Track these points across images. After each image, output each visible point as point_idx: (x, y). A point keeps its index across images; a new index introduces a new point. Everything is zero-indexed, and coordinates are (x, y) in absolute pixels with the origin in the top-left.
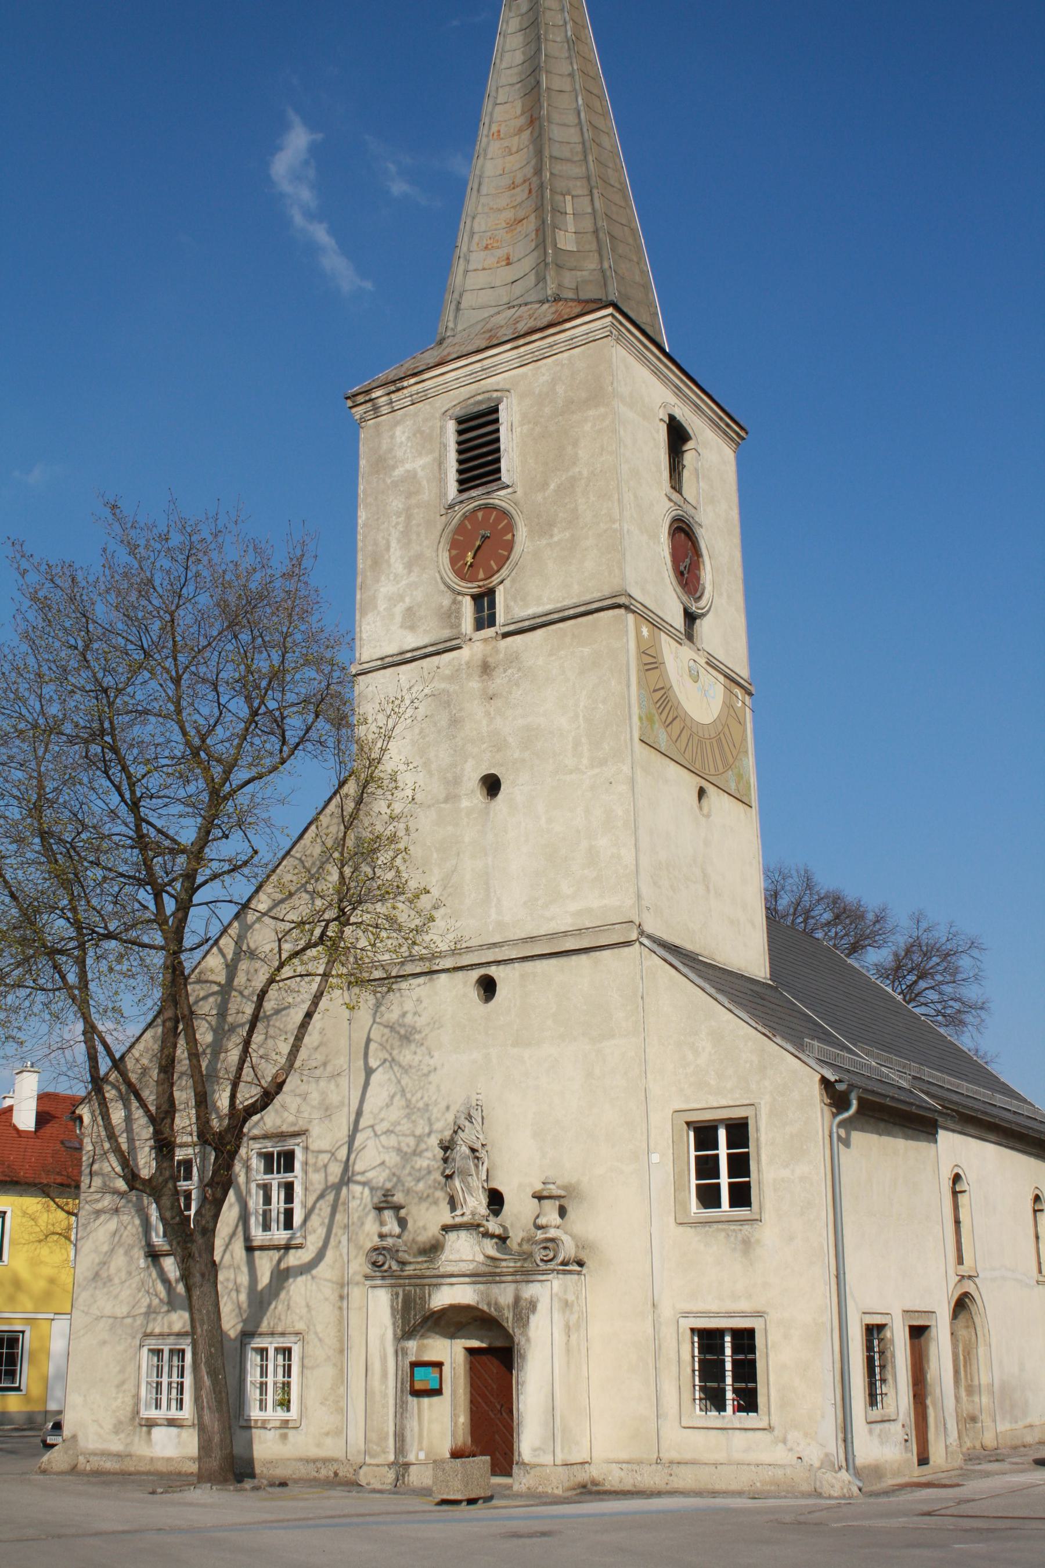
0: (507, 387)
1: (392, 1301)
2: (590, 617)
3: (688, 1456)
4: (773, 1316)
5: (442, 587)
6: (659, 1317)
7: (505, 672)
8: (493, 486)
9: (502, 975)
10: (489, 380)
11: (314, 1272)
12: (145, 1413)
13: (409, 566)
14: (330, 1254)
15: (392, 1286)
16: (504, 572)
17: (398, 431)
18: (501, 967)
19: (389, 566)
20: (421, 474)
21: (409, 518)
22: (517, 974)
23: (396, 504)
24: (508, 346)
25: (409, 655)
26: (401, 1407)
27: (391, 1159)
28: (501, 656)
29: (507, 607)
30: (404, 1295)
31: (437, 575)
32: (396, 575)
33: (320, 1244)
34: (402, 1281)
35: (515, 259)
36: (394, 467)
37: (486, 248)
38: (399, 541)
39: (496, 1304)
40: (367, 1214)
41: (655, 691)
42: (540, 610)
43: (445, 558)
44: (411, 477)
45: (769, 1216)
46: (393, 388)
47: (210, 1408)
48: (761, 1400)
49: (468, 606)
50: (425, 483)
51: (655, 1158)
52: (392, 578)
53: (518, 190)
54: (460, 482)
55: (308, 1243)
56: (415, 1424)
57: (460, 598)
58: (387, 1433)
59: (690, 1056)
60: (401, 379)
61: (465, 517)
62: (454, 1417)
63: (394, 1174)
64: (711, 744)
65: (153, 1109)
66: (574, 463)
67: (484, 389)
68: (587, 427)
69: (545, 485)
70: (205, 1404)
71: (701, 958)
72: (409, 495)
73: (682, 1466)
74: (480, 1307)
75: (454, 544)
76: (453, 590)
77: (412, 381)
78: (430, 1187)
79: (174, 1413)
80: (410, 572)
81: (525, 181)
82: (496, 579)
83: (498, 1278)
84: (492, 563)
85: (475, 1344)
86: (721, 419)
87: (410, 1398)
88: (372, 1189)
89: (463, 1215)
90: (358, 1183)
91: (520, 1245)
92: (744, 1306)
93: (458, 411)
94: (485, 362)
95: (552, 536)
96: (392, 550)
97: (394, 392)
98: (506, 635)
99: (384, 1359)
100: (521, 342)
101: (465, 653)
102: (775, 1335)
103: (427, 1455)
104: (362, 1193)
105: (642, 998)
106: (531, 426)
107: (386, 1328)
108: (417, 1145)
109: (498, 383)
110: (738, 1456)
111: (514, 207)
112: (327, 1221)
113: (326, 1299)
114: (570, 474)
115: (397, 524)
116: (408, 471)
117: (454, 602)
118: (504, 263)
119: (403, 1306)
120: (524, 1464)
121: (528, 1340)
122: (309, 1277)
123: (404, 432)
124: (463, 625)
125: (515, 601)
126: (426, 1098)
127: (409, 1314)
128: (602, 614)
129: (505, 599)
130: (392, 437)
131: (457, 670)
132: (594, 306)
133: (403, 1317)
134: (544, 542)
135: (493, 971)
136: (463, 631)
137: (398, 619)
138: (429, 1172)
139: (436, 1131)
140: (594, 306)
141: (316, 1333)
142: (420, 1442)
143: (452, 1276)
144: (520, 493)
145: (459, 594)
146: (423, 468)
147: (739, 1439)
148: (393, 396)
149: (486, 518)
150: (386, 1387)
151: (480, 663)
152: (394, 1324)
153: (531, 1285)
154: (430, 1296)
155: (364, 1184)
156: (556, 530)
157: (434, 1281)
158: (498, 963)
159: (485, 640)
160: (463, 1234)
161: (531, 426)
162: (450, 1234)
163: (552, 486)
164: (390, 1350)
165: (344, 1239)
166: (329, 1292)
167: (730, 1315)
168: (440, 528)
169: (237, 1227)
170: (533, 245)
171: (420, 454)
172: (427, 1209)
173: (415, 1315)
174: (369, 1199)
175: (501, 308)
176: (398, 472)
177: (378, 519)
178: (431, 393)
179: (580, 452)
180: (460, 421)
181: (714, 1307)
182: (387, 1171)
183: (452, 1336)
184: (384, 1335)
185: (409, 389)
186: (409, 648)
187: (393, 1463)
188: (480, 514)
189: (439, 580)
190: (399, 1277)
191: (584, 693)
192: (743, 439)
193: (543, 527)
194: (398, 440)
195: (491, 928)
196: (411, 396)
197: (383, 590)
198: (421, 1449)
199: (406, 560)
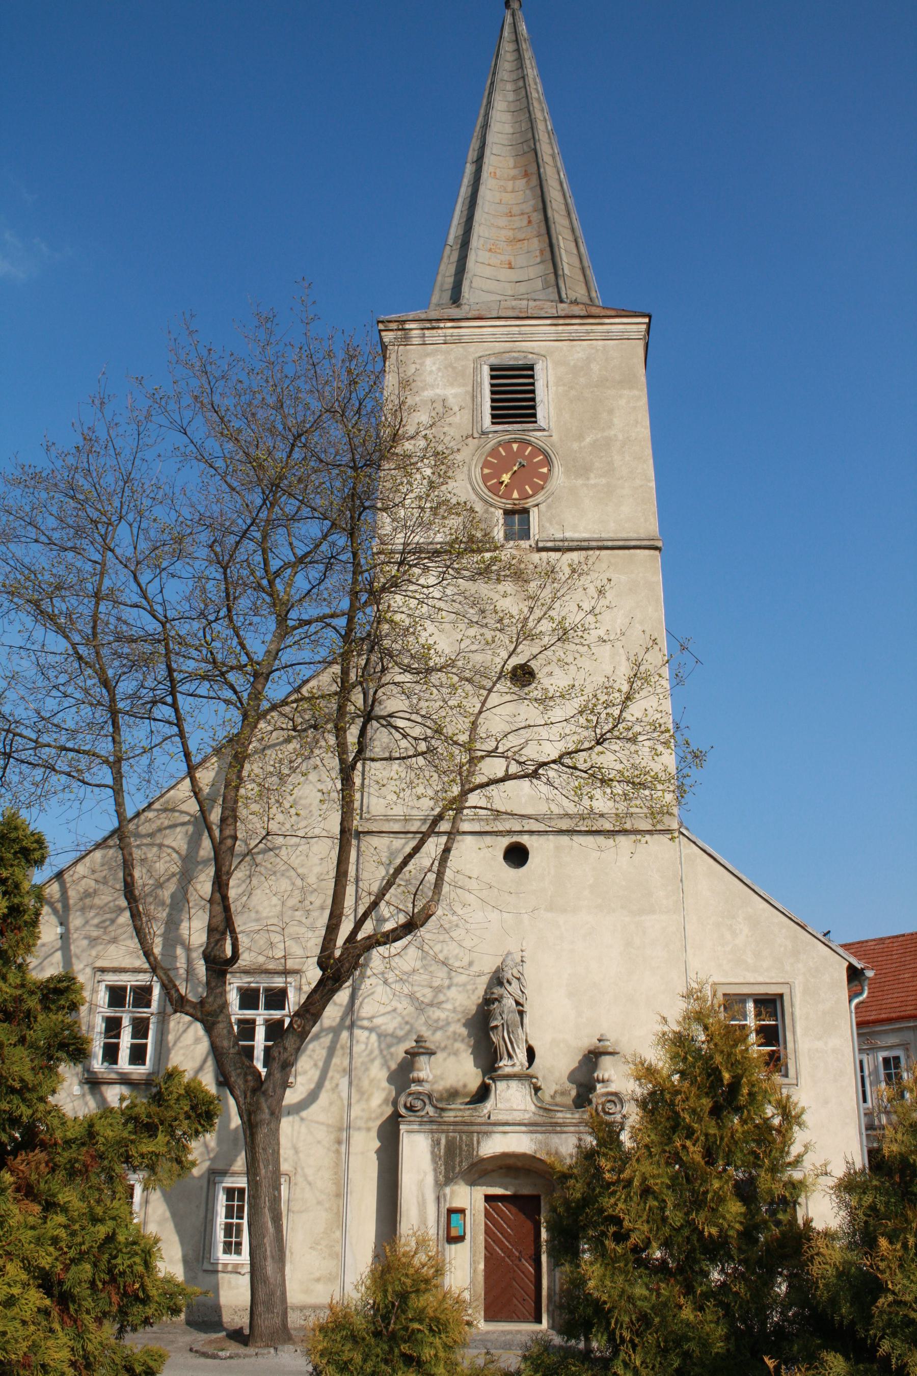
0: (543, 353)
1: (433, 1147)
2: (626, 552)
9: (535, 845)
10: (523, 343)
11: (304, 1114)
14: (324, 1097)
15: (432, 1132)
16: (539, 498)
18: (535, 838)
22: (552, 846)
24: (548, 322)
27: (404, 1006)
30: (448, 1142)
31: (469, 486)
33: (312, 1086)
34: (445, 1127)
36: (424, 389)
39: (557, 1153)
40: (373, 1060)
46: (428, 325)
47: (273, 1257)
54: (494, 416)
55: (298, 1082)
60: (438, 320)
61: (499, 444)
62: (473, 1263)
63: (407, 1023)
65: (360, 936)
67: (519, 349)
68: (622, 402)
69: (580, 437)
70: (268, 1253)
74: (538, 1156)
77: (449, 324)
78: (448, 1038)
82: (530, 502)
83: (558, 1129)
85: (498, 1191)
87: (447, 1246)
88: (379, 1036)
89: (513, 1065)
90: (362, 1028)
91: (553, 1097)
93: (494, 361)
94: (523, 328)
95: (588, 479)
97: (428, 329)
99: (422, 1205)
100: (561, 321)
104: (368, 1038)
105: (681, 881)
106: (566, 388)
107: (425, 1173)
108: (435, 996)
109: (533, 348)
111: (513, 229)
112: (321, 1064)
113: (319, 1142)
114: (606, 434)
117: (486, 511)
119: (446, 1152)
122: (297, 1118)
125: (551, 524)
126: (445, 952)
127: (453, 1160)
128: (638, 551)
132: (613, 313)
133: (446, 1164)
134: (580, 482)
135: (525, 840)
138: (448, 1024)
139: (457, 985)
140: (613, 313)
141: (305, 1177)
143: (506, 1124)
144: (555, 438)
145: (491, 505)
146: (455, 396)
148: (426, 332)
149: (521, 451)
152: (435, 1170)
154: (478, 1143)
155: (371, 1030)
156: (592, 475)
157: (490, 1128)
158: (531, 832)
160: (514, 1084)
161: (566, 388)
162: (498, 1083)
163: (588, 440)
165: (344, 1082)
166: (324, 1136)
169: (205, 1061)
170: (538, 260)
171: (452, 385)
172: (445, 1059)
173: (461, 1162)
174: (376, 1044)
178: (465, 339)
179: (615, 420)
182: (399, 1019)
184: (423, 1180)
185: (444, 331)
188: (515, 446)
190: (440, 1123)
193: (582, 470)
195: (523, 800)
196: (445, 336)
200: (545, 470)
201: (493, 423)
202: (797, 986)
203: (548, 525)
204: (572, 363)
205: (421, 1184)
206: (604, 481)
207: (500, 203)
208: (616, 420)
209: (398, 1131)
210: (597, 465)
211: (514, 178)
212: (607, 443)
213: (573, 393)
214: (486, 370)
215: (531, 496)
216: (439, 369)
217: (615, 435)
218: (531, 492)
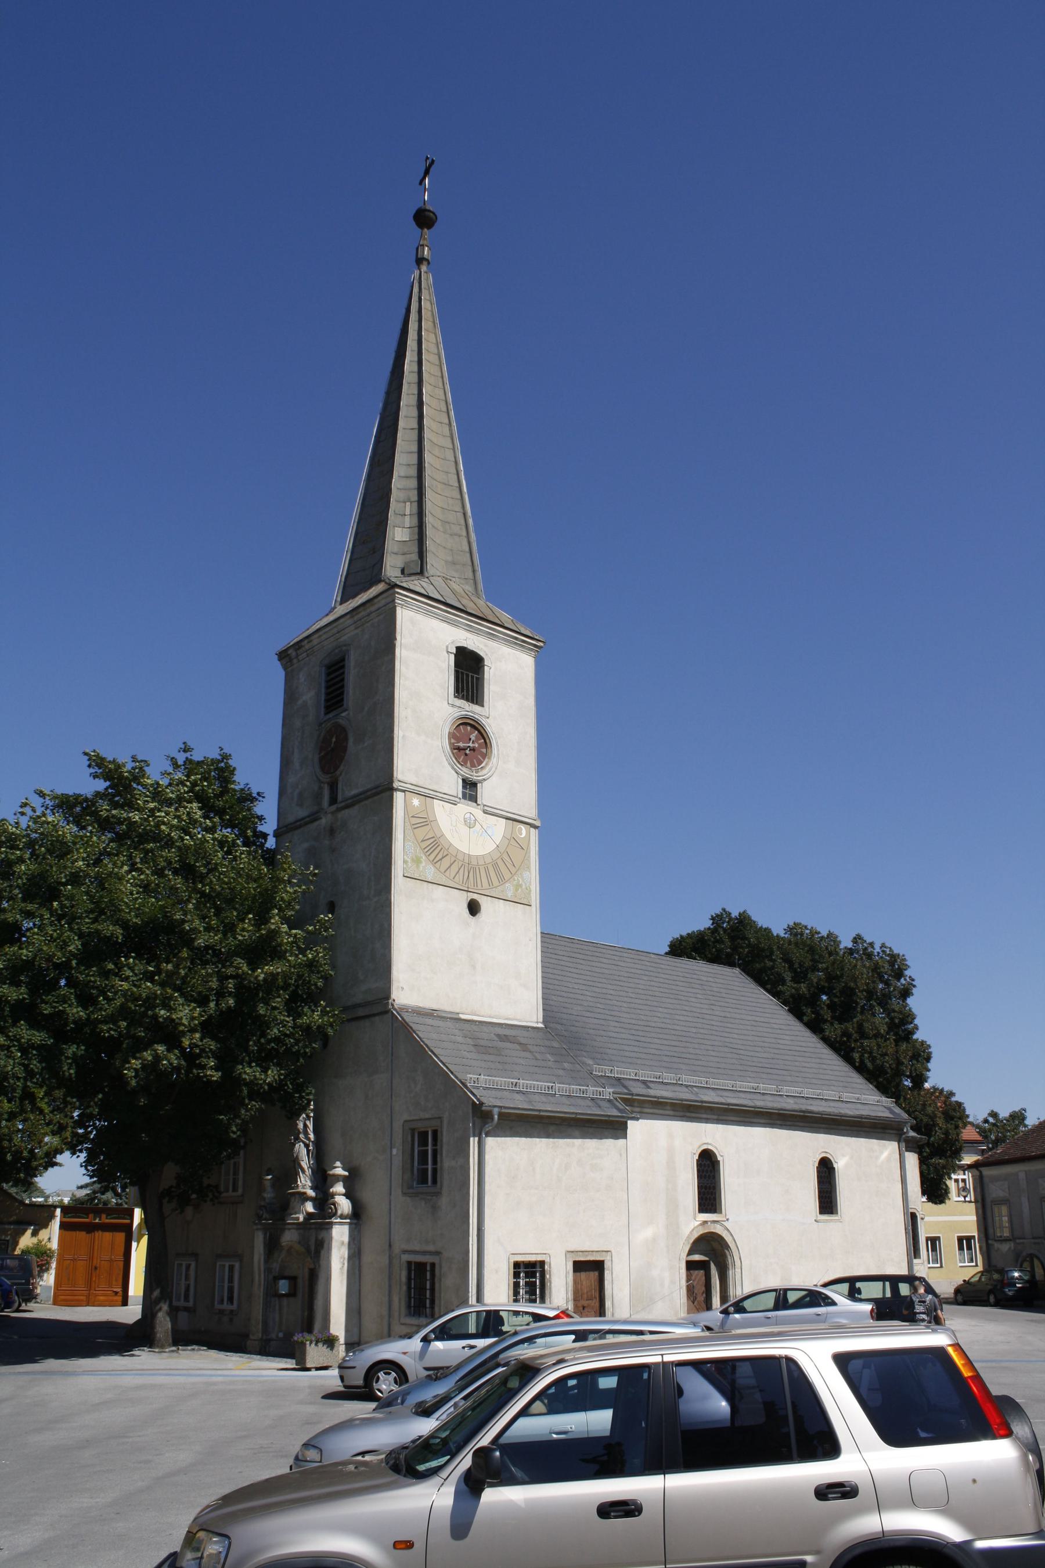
8: (340, 709)
12: (217, 1306)
41: (422, 841)
45: (445, 1191)
51: (394, 1151)
57: (322, 785)
64: (487, 870)
71: (462, 1016)
76: (319, 780)
79: (186, 1304)
86: (516, 638)
92: (431, 1248)
121: (319, 1266)
145: (322, 782)
163: (366, 709)
176: (300, 702)
192: (541, 647)
198: (281, 1331)
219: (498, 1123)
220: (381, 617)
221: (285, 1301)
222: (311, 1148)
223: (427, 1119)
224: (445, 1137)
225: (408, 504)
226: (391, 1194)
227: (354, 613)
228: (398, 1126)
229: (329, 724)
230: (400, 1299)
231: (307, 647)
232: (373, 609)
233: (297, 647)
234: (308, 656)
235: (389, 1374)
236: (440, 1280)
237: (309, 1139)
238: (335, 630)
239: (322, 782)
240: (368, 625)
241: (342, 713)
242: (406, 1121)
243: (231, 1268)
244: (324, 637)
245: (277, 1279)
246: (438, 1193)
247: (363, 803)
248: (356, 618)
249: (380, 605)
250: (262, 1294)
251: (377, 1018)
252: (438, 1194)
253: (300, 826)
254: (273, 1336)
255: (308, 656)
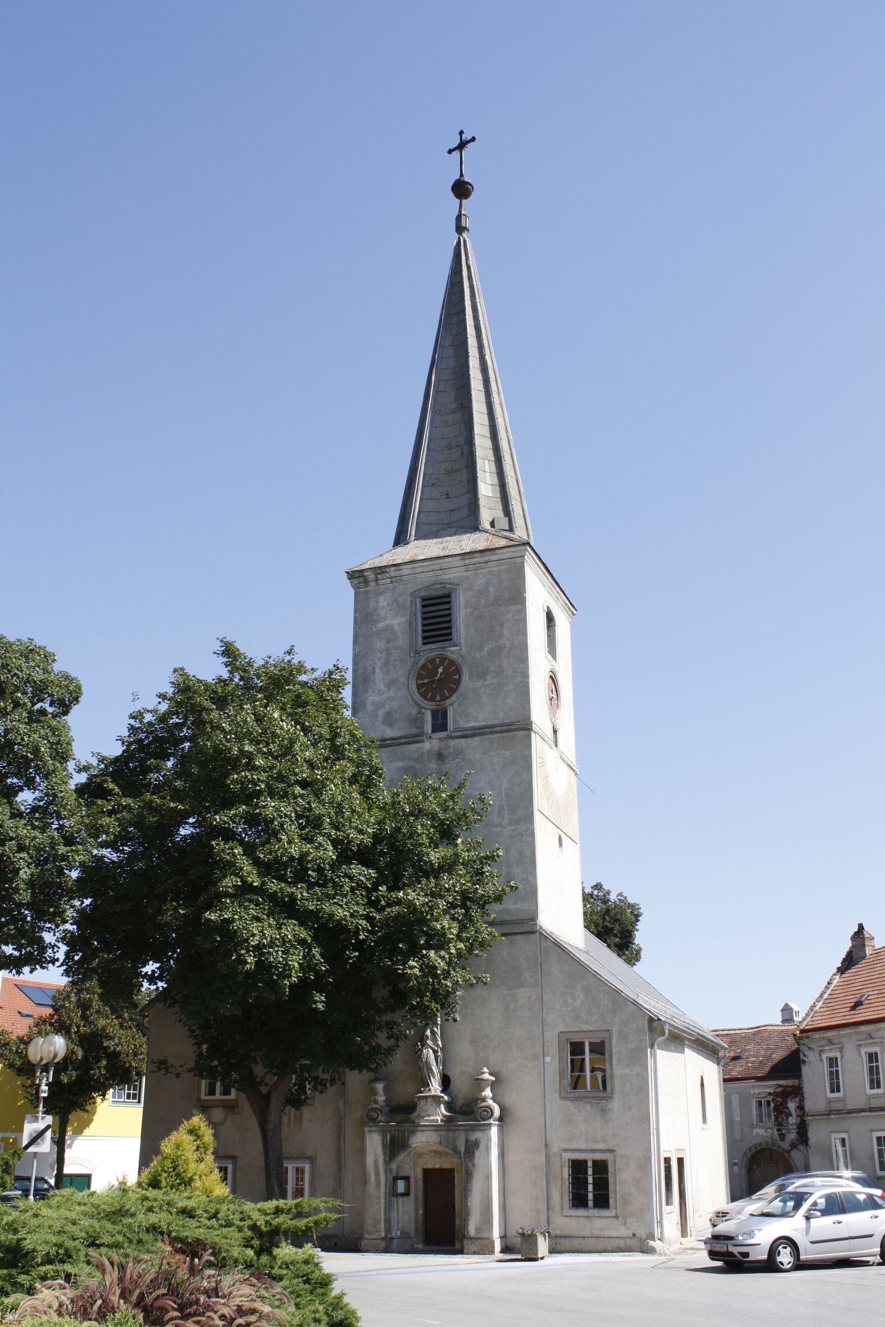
1: (383, 1140)
3: (567, 1233)
4: (619, 1152)
5: (411, 702)
6: (549, 1152)
7: (453, 760)
13: (389, 686)
16: (454, 698)
17: (381, 598)
19: (375, 683)
20: (396, 628)
21: (389, 655)
23: (380, 645)
25: (389, 742)
26: (389, 1204)
28: (451, 750)
29: (455, 721)
31: (408, 694)
32: (379, 691)
35: (452, 496)
36: (378, 622)
37: (433, 485)
38: (381, 669)
42: (477, 724)
43: (413, 685)
44: (390, 629)
45: (616, 1095)
48: (611, 1201)
49: (428, 717)
50: (399, 634)
51: (548, 1059)
52: (376, 691)
53: (453, 450)
54: (424, 638)
56: (395, 1214)
58: (380, 1219)
59: (570, 1001)
62: (416, 1210)
66: (501, 637)
68: (510, 616)
69: (481, 649)
72: (388, 641)
73: (563, 1239)
75: (419, 677)
76: (419, 705)
80: (389, 689)
81: (458, 446)
82: (448, 702)
84: (446, 691)
93: (423, 593)
95: (485, 680)
96: (377, 674)
98: (452, 738)
101: (427, 745)
102: (620, 1163)
103: (401, 1233)
109: (450, 579)
110: (597, 1233)
111: (451, 461)
114: (498, 643)
115: (380, 658)
116: (388, 626)
117: (420, 712)
118: (445, 497)
120: (471, 1238)
121: (474, 1165)
123: (385, 600)
124: (425, 728)
125: (461, 718)
129: (454, 715)
130: (377, 602)
131: (421, 755)
133: (390, 1150)
134: (480, 683)
136: (426, 731)
137: (381, 718)
142: (398, 1226)
144: (464, 650)
145: (423, 708)
146: (399, 625)
147: (598, 1223)
150: (379, 1192)
151: (436, 753)
152: (384, 1154)
153: (476, 1133)
154: (408, 1137)
156: (488, 677)
159: (440, 739)
163: (486, 649)
164: (382, 1169)
167: (593, 1151)
168: (410, 664)
170: (466, 490)
171: (396, 616)
175: (444, 526)
176: (381, 625)
177: (367, 653)
179: (504, 631)
180: (424, 600)
181: (583, 1146)
183: (177, 1129)
186: (388, 737)
187: (384, 1238)
189: (409, 697)
191: (506, 779)
193: (480, 673)
194: (381, 605)
197: (371, 699)
198: (398, 1230)
199: (386, 681)
200: (457, 677)
201: (424, 644)
202: (614, 1032)
203: (459, 718)
204: (476, 588)
205: (376, 1162)
206: (496, 681)
207: (443, 438)
208: (505, 632)
209: (364, 1131)
210: (492, 668)
211: (454, 412)
212: (500, 648)
213: (477, 612)
214: (418, 600)
215: (448, 698)
216: (388, 604)
217: (504, 644)
218: (447, 695)
219: (667, 1039)
220: (503, 567)
221: (400, 1199)
222: (439, 1054)
223: (591, 1031)
224: (616, 1048)
225: (486, 461)
226: (545, 1098)
227: (467, 557)
228: (552, 1037)
229: (432, 654)
230: (562, 1194)
231: (393, 574)
232: (494, 558)
233: (379, 571)
234: (392, 582)
235: (779, 1252)
236: (615, 1175)
237: (438, 1045)
238: (438, 567)
239: (423, 708)
240: (485, 571)
241: (450, 647)
242: (560, 1032)
243: (299, 1171)
244: (420, 570)
245: (396, 1179)
246: (609, 1097)
247: (487, 736)
248: (467, 562)
249: (504, 556)
250: (382, 1195)
251: (519, 937)
252: (610, 1098)
253: (391, 745)
254: (394, 1235)
255: (392, 582)
